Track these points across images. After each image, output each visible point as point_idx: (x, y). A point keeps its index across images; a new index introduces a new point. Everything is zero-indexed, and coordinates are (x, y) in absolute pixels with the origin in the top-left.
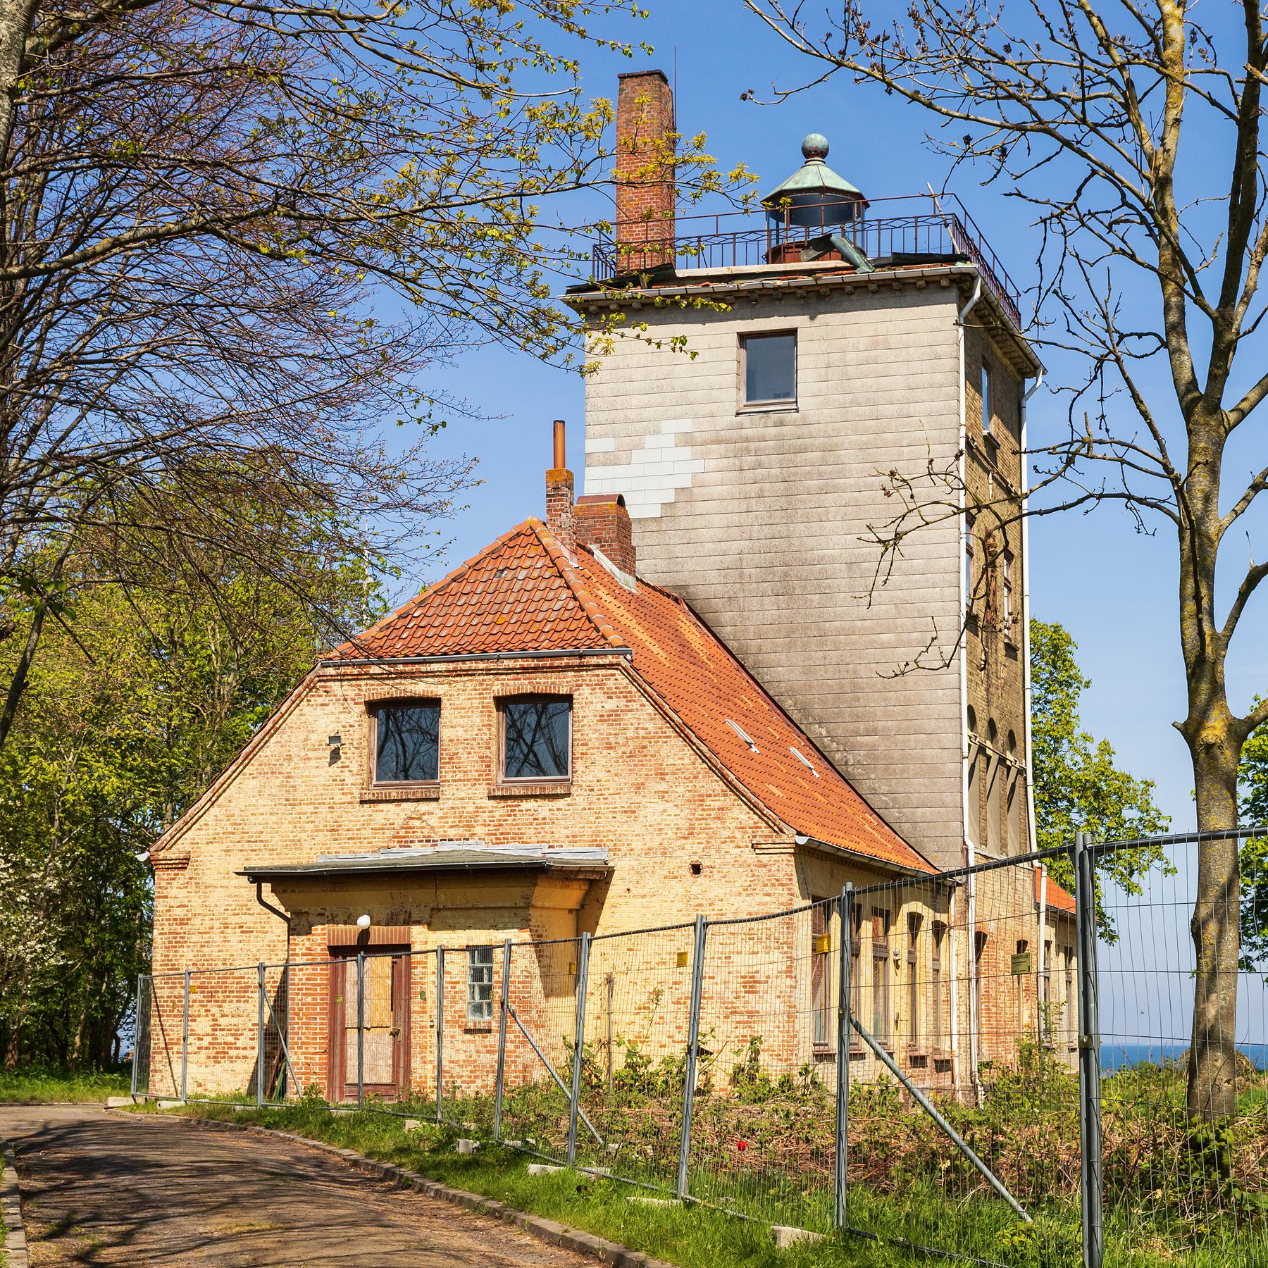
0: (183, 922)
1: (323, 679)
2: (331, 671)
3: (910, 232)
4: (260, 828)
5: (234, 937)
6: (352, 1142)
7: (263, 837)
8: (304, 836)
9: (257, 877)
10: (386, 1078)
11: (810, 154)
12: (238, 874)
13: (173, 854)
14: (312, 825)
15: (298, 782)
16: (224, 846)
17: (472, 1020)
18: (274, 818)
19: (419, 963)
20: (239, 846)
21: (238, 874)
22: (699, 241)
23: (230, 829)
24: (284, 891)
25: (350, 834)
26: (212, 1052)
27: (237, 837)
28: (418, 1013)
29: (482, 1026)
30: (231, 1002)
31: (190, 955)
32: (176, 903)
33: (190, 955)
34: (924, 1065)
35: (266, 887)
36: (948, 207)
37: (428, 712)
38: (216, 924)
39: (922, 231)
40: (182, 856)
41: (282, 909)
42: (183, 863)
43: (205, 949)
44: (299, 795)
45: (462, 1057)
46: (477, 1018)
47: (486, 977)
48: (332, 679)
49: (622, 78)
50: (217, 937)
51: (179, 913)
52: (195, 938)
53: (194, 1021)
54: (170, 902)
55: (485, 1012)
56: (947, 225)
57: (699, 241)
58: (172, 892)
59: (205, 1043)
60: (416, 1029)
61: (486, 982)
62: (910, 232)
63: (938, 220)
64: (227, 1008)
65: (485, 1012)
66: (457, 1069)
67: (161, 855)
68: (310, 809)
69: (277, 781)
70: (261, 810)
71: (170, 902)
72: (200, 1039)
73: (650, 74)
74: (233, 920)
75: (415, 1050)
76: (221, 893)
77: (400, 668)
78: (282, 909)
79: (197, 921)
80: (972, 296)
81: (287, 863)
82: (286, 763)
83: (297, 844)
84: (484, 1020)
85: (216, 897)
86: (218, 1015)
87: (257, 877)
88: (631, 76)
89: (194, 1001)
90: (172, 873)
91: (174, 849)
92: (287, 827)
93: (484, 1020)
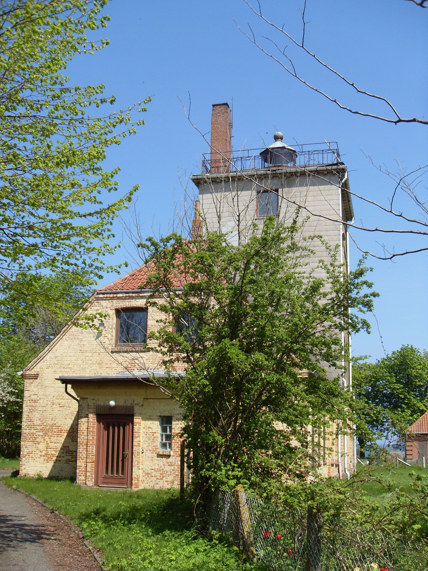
0: (35, 401)
1: (98, 299)
2: (101, 296)
3: (321, 155)
4: (68, 362)
5: (57, 408)
6: (108, 566)
7: (70, 366)
8: (87, 366)
9: (65, 381)
10: (68, 385)
11: (276, 138)
12: (56, 379)
13: (32, 372)
14: (90, 362)
15: (85, 343)
16: (53, 370)
17: (161, 451)
18: (75, 358)
19: (137, 423)
20: (60, 370)
21: (56, 379)
22: (241, 159)
23: (56, 362)
24: (77, 388)
25: (107, 366)
26: (46, 458)
27: (59, 366)
28: (136, 446)
29: (167, 453)
30: (54, 437)
31: (38, 416)
32: (33, 393)
33: (38, 416)
34: (164, 445)
35: (69, 386)
36: (333, 147)
37: (142, 314)
38: (49, 403)
39: (325, 155)
40: (36, 373)
41: (76, 396)
42: (36, 377)
43: (44, 413)
44: (86, 348)
45: (157, 467)
46: (164, 450)
47: (168, 430)
48: (102, 299)
49: (213, 106)
50: (49, 408)
51: (34, 397)
52: (40, 409)
53: (39, 444)
54: (31, 393)
55: (168, 446)
56: (334, 153)
57: (241, 159)
58: (31, 388)
59: (43, 454)
60: (135, 454)
61: (168, 433)
62: (321, 155)
63: (331, 151)
64: (53, 439)
65: (168, 446)
66: (154, 473)
67: (28, 372)
68: (90, 354)
69: (76, 342)
70: (69, 354)
71: (31, 393)
72: (41, 452)
73: (224, 104)
74: (56, 401)
75: (135, 463)
76: (51, 390)
77: (131, 295)
78: (76, 396)
79: (41, 401)
80: (344, 177)
81: (78, 375)
82: (80, 335)
83: (84, 369)
84: (167, 451)
85: (50, 391)
86: (49, 442)
87: (65, 381)
88: (217, 105)
89: (39, 436)
90: (32, 380)
91: (33, 371)
92: (80, 362)
93: (167, 451)
